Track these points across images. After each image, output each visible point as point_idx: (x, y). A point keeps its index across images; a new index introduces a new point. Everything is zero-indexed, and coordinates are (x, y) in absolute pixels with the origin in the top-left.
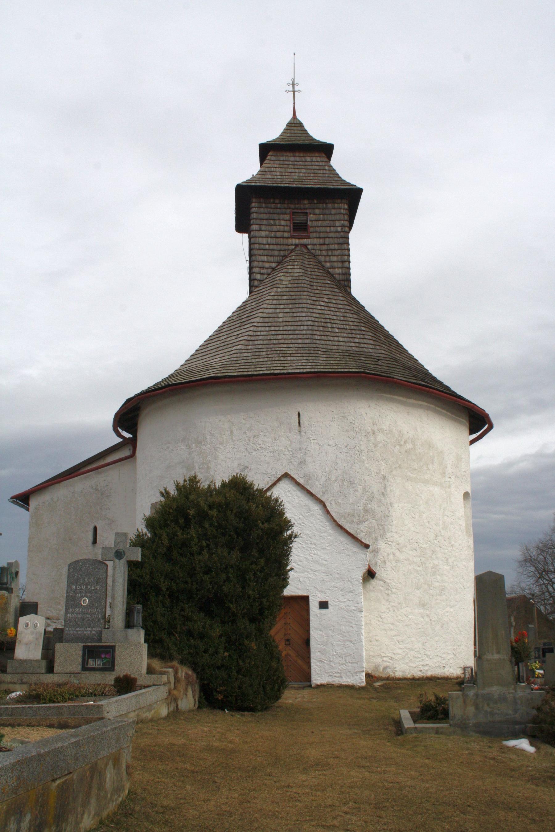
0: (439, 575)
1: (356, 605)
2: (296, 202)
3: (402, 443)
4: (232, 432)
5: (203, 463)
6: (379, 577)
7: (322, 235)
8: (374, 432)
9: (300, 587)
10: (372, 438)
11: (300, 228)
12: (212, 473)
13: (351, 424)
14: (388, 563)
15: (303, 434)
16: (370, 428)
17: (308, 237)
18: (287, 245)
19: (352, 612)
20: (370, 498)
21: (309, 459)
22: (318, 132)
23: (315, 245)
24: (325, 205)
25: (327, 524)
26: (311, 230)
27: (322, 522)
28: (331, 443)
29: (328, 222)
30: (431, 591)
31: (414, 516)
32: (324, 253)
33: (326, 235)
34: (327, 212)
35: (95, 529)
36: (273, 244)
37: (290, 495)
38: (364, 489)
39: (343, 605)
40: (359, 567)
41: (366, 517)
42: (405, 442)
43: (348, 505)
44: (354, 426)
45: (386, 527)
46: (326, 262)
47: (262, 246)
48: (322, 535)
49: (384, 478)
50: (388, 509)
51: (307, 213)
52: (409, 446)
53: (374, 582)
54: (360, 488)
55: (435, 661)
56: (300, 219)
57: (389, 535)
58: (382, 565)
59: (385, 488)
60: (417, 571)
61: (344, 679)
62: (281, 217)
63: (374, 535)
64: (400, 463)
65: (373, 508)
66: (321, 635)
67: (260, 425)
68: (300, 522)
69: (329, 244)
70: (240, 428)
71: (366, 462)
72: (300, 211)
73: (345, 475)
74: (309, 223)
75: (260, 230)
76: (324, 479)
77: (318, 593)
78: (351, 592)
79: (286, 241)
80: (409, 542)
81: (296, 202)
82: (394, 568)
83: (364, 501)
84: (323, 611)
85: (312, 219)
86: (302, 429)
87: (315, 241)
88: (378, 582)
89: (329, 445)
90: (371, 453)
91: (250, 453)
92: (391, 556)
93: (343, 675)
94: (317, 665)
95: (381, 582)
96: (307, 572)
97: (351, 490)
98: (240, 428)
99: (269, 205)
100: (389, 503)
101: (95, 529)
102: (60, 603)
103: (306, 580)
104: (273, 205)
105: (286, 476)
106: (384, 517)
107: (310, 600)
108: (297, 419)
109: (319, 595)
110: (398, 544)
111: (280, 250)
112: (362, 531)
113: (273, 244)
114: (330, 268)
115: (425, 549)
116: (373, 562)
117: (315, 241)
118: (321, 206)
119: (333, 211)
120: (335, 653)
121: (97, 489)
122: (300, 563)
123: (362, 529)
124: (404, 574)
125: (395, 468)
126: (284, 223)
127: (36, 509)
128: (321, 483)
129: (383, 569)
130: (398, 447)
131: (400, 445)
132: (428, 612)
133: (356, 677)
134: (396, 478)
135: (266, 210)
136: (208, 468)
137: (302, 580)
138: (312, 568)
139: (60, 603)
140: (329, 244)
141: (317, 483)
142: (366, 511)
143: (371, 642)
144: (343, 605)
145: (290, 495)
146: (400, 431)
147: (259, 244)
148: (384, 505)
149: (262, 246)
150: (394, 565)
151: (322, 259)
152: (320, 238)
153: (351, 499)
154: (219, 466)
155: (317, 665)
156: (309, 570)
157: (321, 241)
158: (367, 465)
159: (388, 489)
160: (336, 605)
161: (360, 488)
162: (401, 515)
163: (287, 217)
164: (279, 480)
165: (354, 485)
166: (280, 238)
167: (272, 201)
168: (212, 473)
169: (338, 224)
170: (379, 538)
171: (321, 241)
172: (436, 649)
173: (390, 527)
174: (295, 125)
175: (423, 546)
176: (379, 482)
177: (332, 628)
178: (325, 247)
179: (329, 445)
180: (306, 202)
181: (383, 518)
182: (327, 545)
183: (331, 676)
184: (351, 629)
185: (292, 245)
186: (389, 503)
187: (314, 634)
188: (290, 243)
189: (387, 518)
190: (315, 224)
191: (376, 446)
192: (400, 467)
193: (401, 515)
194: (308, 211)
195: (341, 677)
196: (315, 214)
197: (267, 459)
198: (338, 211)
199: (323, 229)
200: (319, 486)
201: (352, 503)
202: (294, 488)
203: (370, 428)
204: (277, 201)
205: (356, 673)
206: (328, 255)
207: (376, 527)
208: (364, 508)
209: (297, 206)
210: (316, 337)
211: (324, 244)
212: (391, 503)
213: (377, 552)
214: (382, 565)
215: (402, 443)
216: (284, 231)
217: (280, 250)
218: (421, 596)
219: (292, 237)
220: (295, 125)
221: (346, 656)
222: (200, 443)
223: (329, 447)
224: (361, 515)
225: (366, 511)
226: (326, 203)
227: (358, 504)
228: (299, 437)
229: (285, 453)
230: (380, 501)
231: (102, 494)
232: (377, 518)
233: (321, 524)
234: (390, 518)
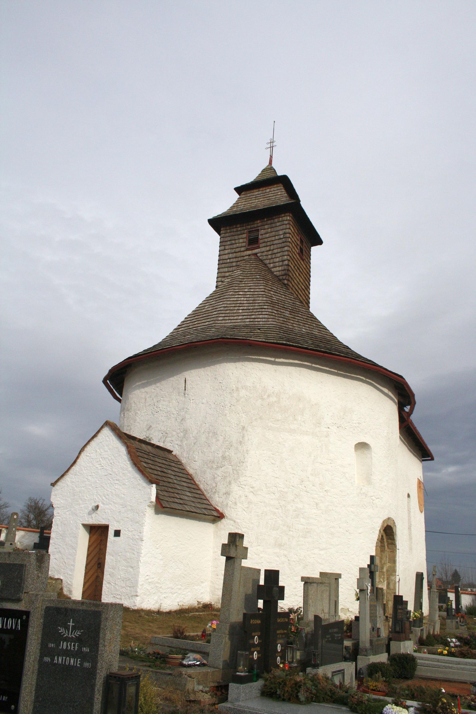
0: (303, 518)
1: (139, 534)
2: (268, 226)
3: (265, 397)
4: (146, 400)
6: (229, 517)
7: (269, 244)
8: (237, 389)
9: (104, 517)
10: (235, 395)
11: (253, 242)
13: (220, 384)
14: (239, 504)
15: (186, 396)
16: (234, 386)
17: (259, 247)
18: (243, 256)
19: (135, 540)
20: (228, 447)
21: (187, 416)
23: (264, 252)
24: (272, 221)
25: (128, 462)
26: (261, 241)
27: (125, 461)
28: (204, 401)
29: (274, 233)
30: (291, 533)
31: (274, 462)
32: (269, 257)
33: (271, 243)
34: (274, 225)
36: (233, 258)
37: (108, 440)
38: (225, 438)
39: (130, 534)
40: (145, 501)
41: (223, 463)
42: (269, 396)
43: (211, 453)
44: (222, 385)
45: (240, 472)
46: (270, 264)
47: (225, 261)
48: (124, 472)
49: (244, 428)
50: (244, 456)
51: (258, 230)
52: (273, 399)
54: (221, 438)
55: (293, 600)
56: (253, 235)
57: (242, 479)
58: (233, 506)
59: (243, 437)
60: (275, 513)
61: (123, 601)
62: (240, 236)
63: (228, 480)
64: (261, 415)
65: (230, 455)
66: (113, 560)
67: (162, 392)
68: (112, 462)
69: (273, 250)
71: (228, 415)
72: (253, 229)
73: (211, 427)
74: (260, 237)
77: (115, 522)
78: (137, 522)
79: (242, 254)
80: (266, 486)
81: (268, 226)
82: (246, 509)
83: (223, 449)
84: (117, 538)
85: (263, 233)
86: (186, 392)
87: (263, 249)
88: (228, 521)
89: (203, 403)
90: (233, 407)
92: (243, 498)
93: (123, 597)
94: (107, 587)
95: (232, 522)
96: (111, 504)
97: (214, 440)
99: (232, 230)
100: (245, 450)
103: (109, 511)
104: (235, 230)
105: (107, 424)
106: (239, 463)
107: (109, 529)
108: (184, 384)
109: (116, 525)
110: (252, 488)
111: (237, 262)
112: (218, 476)
113: (233, 258)
114: (273, 268)
115: (286, 493)
116: (225, 503)
117: (263, 249)
118: (269, 222)
119: (278, 224)
120: (119, 577)
122: (107, 497)
123: (219, 474)
124: (258, 516)
125: (256, 419)
128: (194, 436)
129: (233, 510)
130: (259, 400)
131: (263, 399)
132: (285, 552)
133: (131, 600)
134: (256, 428)
135: (230, 234)
137: (106, 511)
138: (114, 501)
140: (273, 250)
141: (191, 436)
142: (224, 458)
143: (217, 575)
144: (130, 534)
145: (108, 440)
146: (264, 387)
147: (223, 260)
148: (240, 452)
149: (225, 261)
150: (247, 506)
151: (267, 262)
152: (267, 246)
153: (213, 448)
154: (136, 427)
155: (107, 587)
156: (112, 503)
157: (268, 248)
158: (229, 418)
159: (246, 438)
160: (126, 534)
161: (221, 438)
162: (259, 461)
163: (244, 236)
164: (102, 427)
165: (216, 436)
166: (238, 252)
167: (234, 227)
169: (281, 232)
170: (233, 482)
171: (268, 248)
172: (295, 588)
173: (244, 472)
174: (270, 168)
175: (283, 490)
176: (238, 433)
177: (120, 554)
178: (270, 253)
179: (203, 403)
180: (258, 222)
181: (238, 464)
182: (127, 481)
183: (114, 597)
184: (133, 556)
185: (246, 256)
186: (245, 450)
187: (108, 558)
188: (244, 255)
189: (242, 464)
191: (238, 401)
192: (261, 418)
193: (259, 461)
194: (259, 228)
195: (121, 599)
196: (264, 229)
197: (162, 419)
198: (282, 223)
199: (269, 239)
200: (192, 438)
201: (214, 452)
202: (111, 434)
203: (234, 386)
204: (238, 226)
205: (132, 596)
206: (272, 258)
207: (231, 472)
208: (223, 455)
209: (252, 226)
211: (270, 250)
212: (247, 451)
213: (229, 494)
214: (233, 506)
215: (265, 397)
216: (242, 247)
217: (237, 262)
218: (278, 536)
219: (247, 250)
220: (270, 168)
221: (126, 581)
223: (202, 405)
224: (220, 462)
225: (224, 458)
226: (273, 219)
227: (218, 452)
228: (184, 399)
229: (174, 413)
230: (237, 449)
232: (232, 464)
233: (124, 463)
234: (244, 464)
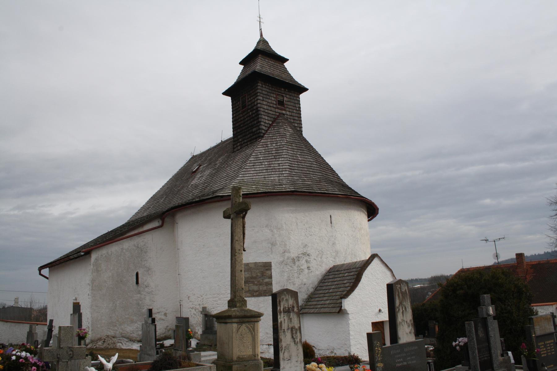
5: (282, 241)
12: (288, 248)
21: (337, 242)
22: (278, 49)
28: (346, 233)
35: (137, 274)
53: (381, 313)
56: (280, 98)
70: (302, 222)
75: (263, 100)
76: (344, 253)
91: (308, 237)
98: (302, 222)
101: (137, 274)
102: (116, 326)
121: (138, 247)
126: (273, 99)
127: (96, 259)
136: (285, 245)
139: (116, 326)
168: (288, 248)
174: (263, 41)
178: (291, 117)
190: (287, 103)
210: (296, 168)
220: (263, 41)
222: (280, 229)
231: (142, 251)
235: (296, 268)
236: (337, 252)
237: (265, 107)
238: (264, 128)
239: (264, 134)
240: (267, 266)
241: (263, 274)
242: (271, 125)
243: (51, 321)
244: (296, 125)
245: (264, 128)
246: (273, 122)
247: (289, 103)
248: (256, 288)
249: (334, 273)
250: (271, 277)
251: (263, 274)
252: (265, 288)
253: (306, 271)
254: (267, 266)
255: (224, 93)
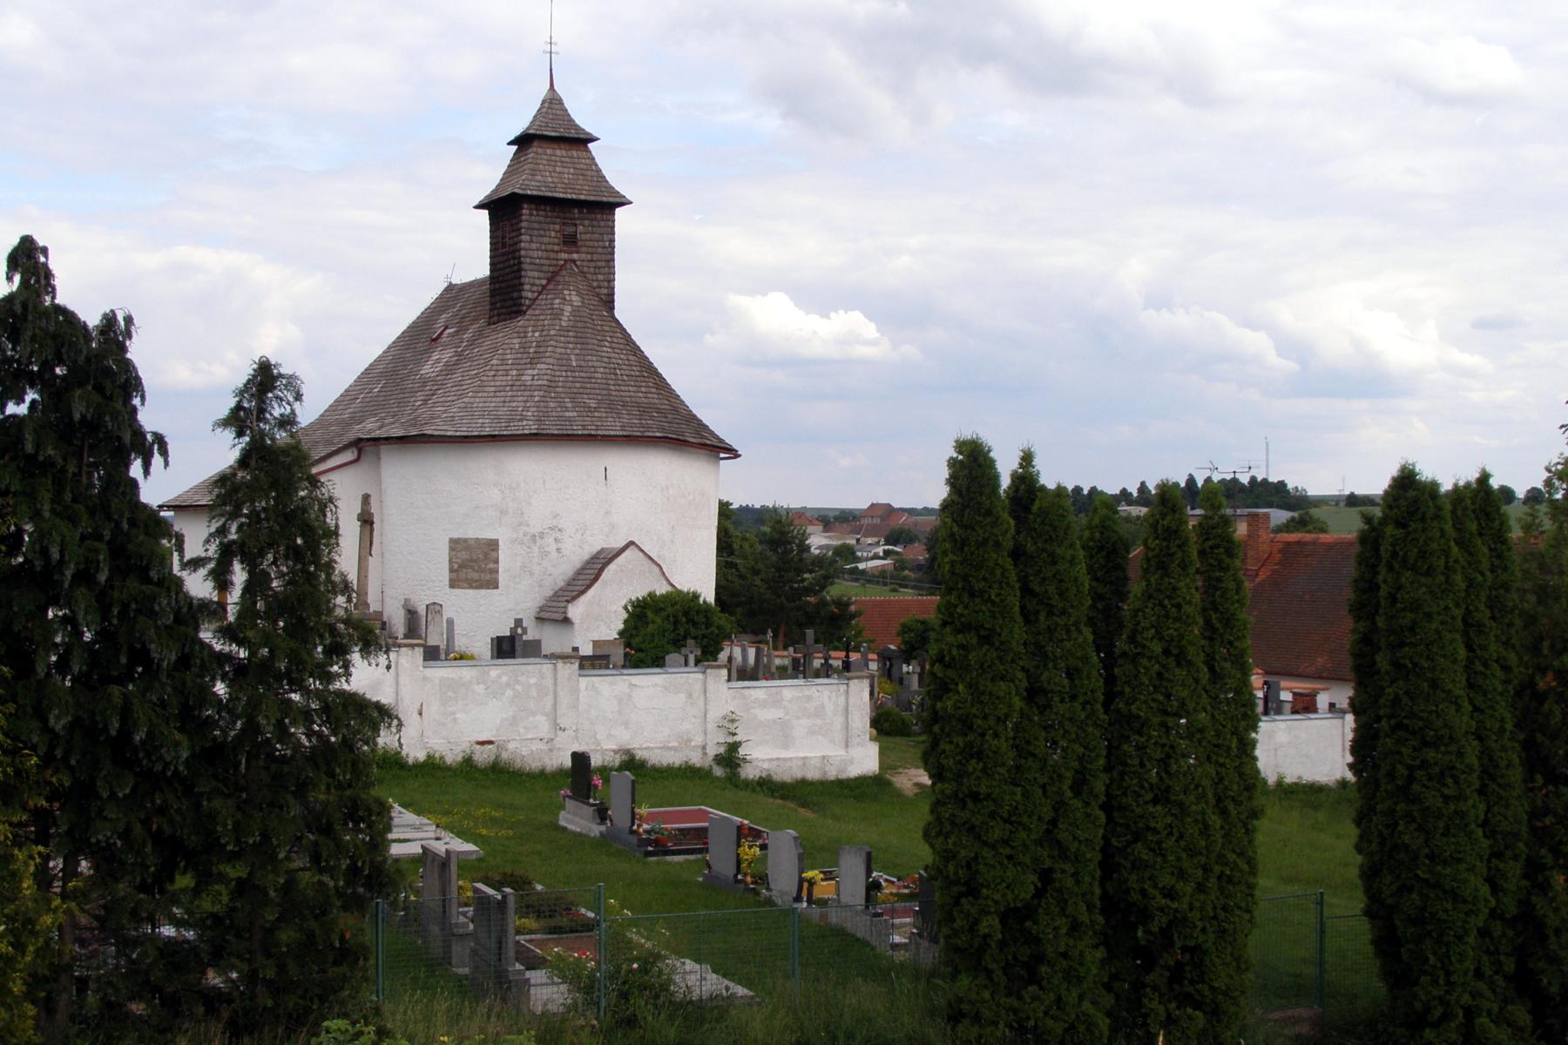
22: (583, 116)
56: (570, 230)
126: (553, 233)
174: (553, 104)
220: (553, 104)
235: (536, 549)
236: (613, 526)
237: (535, 254)
238: (530, 295)
239: (529, 307)
240: (493, 545)
241: (486, 555)
242: (544, 287)
243: (450, 622)
244: (601, 277)
245: (530, 295)
246: (549, 280)
247: (588, 236)
248: (475, 576)
249: (595, 558)
250: (497, 562)
251: (486, 555)
252: (488, 577)
253: (554, 554)
254: (493, 545)
255: (477, 207)
